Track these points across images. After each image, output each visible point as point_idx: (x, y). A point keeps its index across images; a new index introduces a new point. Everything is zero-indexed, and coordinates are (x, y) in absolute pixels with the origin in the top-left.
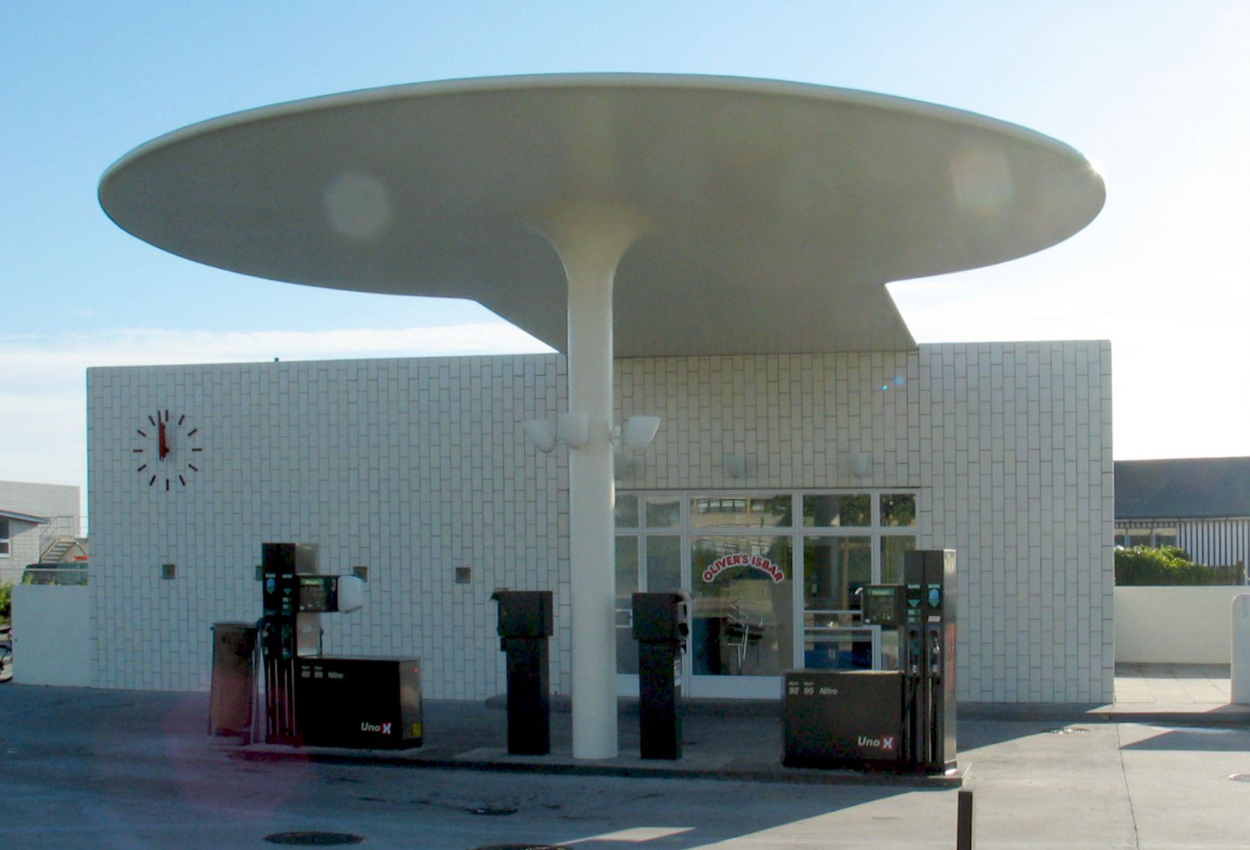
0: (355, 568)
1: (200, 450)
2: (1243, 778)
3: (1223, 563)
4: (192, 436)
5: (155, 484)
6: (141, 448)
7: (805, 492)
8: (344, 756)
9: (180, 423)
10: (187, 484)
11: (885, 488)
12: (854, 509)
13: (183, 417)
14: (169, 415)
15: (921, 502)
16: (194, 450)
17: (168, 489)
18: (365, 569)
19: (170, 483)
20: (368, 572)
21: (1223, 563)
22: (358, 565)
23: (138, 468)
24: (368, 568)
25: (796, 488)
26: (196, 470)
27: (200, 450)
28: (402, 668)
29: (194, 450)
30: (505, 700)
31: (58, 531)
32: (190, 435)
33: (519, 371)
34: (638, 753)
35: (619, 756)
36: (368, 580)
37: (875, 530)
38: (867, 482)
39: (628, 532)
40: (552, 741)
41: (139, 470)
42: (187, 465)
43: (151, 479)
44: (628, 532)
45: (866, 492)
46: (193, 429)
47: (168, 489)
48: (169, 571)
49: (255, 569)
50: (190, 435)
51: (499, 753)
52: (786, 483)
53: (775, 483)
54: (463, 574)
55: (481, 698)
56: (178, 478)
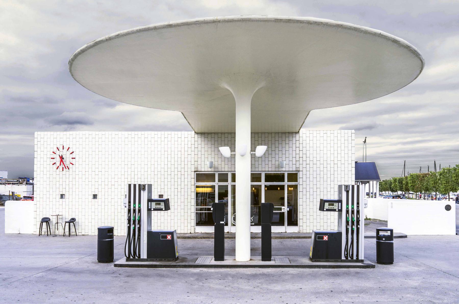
0: (281, 198)
1: (75, 158)
4: (72, 154)
5: (58, 169)
6: (54, 157)
7: (265, 172)
8: (256, 267)
9: (68, 150)
13: (69, 148)
14: (64, 147)
15: (300, 175)
16: (72, 158)
17: (63, 170)
18: (163, 195)
20: (97, 196)
22: (160, 194)
23: (53, 164)
24: (98, 195)
25: (263, 171)
26: (73, 164)
27: (75, 158)
28: (148, 230)
29: (72, 158)
31: (453, 193)
32: (71, 154)
33: (263, 142)
34: (260, 257)
38: (284, 169)
39: (233, 183)
41: (53, 164)
42: (70, 163)
43: (57, 167)
44: (233, 183)
47: (63, 170)
49: (92, 195)
50: (71, 154)
51: (306, 261)
53: (257, 170)
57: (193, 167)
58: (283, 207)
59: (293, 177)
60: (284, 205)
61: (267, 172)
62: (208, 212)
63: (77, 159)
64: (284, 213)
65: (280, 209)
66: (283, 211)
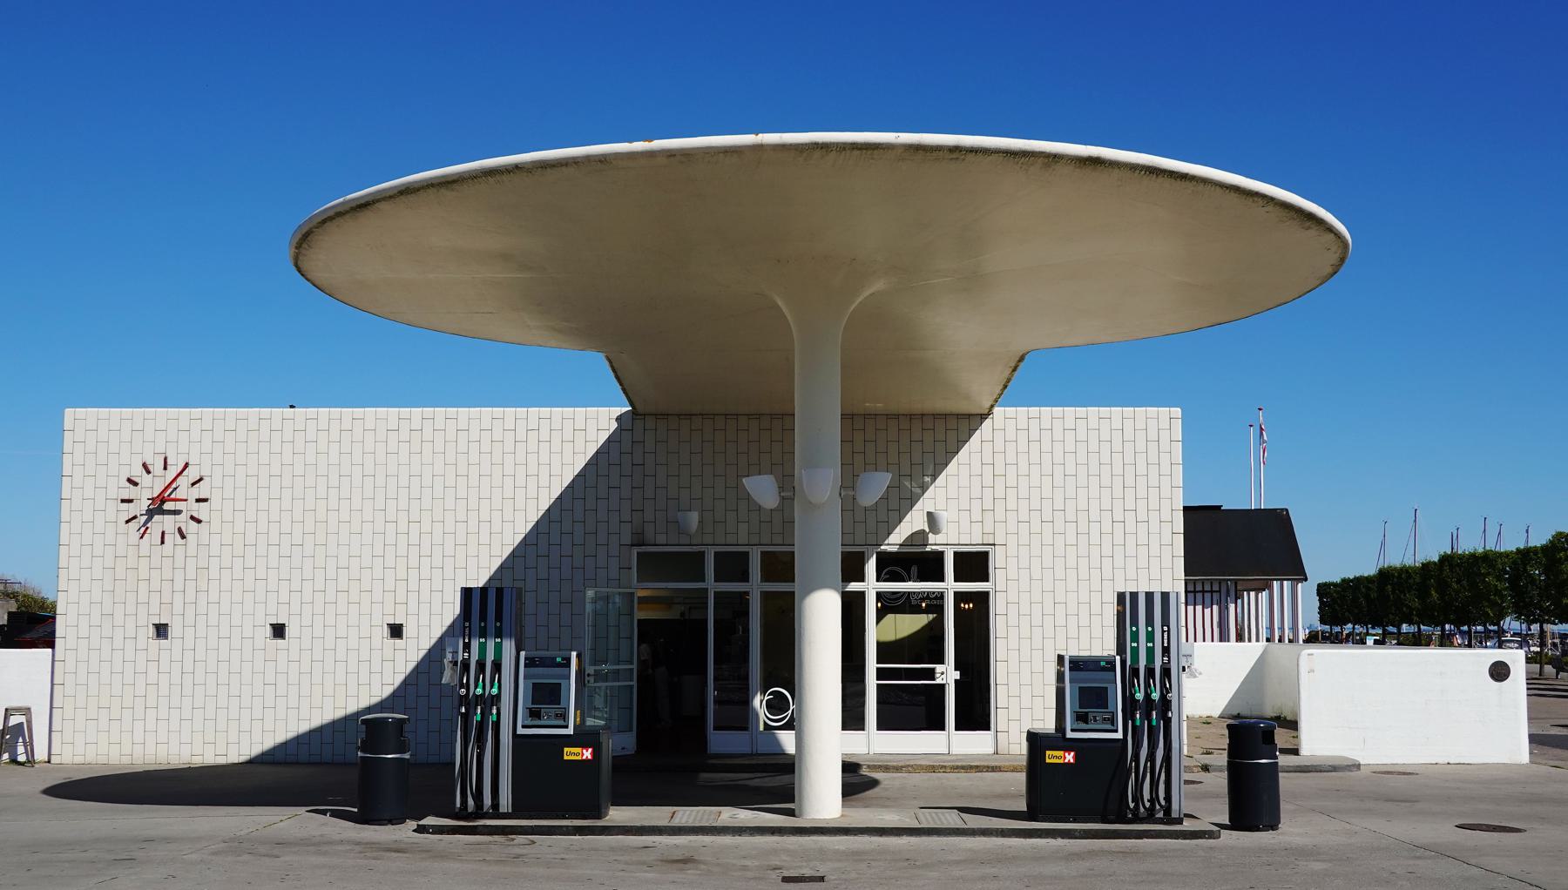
2: (1491, 829)
3: (1207, 611)
10: (188, 536)
11: (983, 545)
12: (690, 564)
15: (997, 561)
17: (163, 542)
19: (166, 536)
21: (1207, 611)
30: (1024, 762)
32: (193, 484)
35: (842, 816)
36: (404, 638)
37: (950, 586)
40: (1285, 807)
45: (702, 548)
46: (198, 478)
47: (163, 542)
48: (161, 630)
52: (743, 539)
53: (731, 539)
54: (396, 631)
55: (243, 759)
56: (177, 530)
57: (627, 529)
58: (939, 668)
59: (974, 564)
60: (941, 661)
61: (1106, 710)
62: (705, 621)
63: (215, 501)
64: (942, 687)
65: (931, 674)
66: (938, 681)
